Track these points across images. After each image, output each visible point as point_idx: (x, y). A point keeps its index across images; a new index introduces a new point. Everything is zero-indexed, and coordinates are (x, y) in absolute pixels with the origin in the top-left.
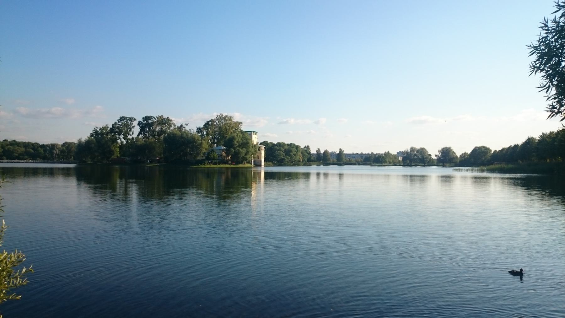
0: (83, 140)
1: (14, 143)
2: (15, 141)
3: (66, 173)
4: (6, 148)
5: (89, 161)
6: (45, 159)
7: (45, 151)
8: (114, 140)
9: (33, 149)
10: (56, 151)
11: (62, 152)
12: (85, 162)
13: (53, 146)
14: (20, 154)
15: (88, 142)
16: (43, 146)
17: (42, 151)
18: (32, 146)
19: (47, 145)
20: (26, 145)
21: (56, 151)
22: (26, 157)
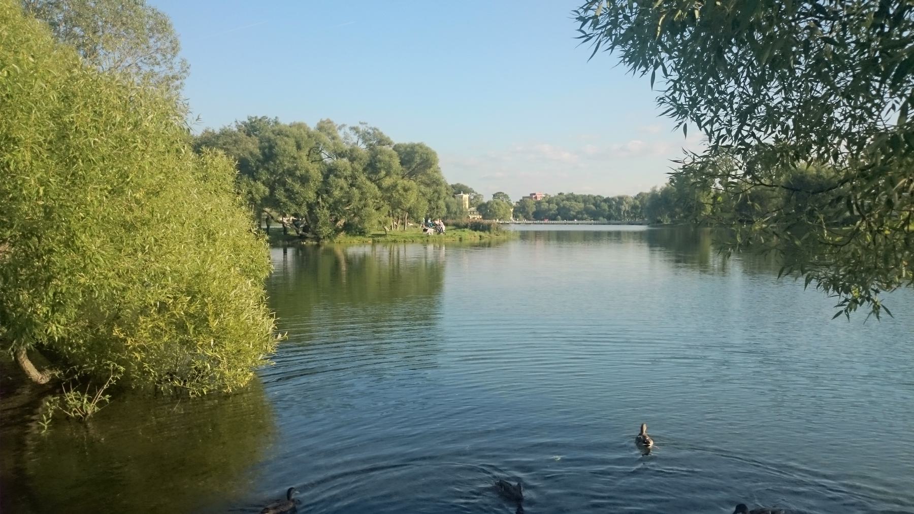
0: (658, 189)
1: (572, 198)
2: (572, 194)
3: (639, 236)
4: (561, 205)
5: (667, 220)
6: (610, 219)
7: (610, 207)
8: (705, 186)
9: (593, 204)
10: (625, 207)
11: (634, 207)
12: (659, 222)
13: (621, 200)
14: (578, 213)
15: (666, 192)
16: (607, 200)
17: (605, 206)
18: (593, 201)
19: (613, 199)
20: (586, 199)
21: (625, 207)
22: (586, 216)
